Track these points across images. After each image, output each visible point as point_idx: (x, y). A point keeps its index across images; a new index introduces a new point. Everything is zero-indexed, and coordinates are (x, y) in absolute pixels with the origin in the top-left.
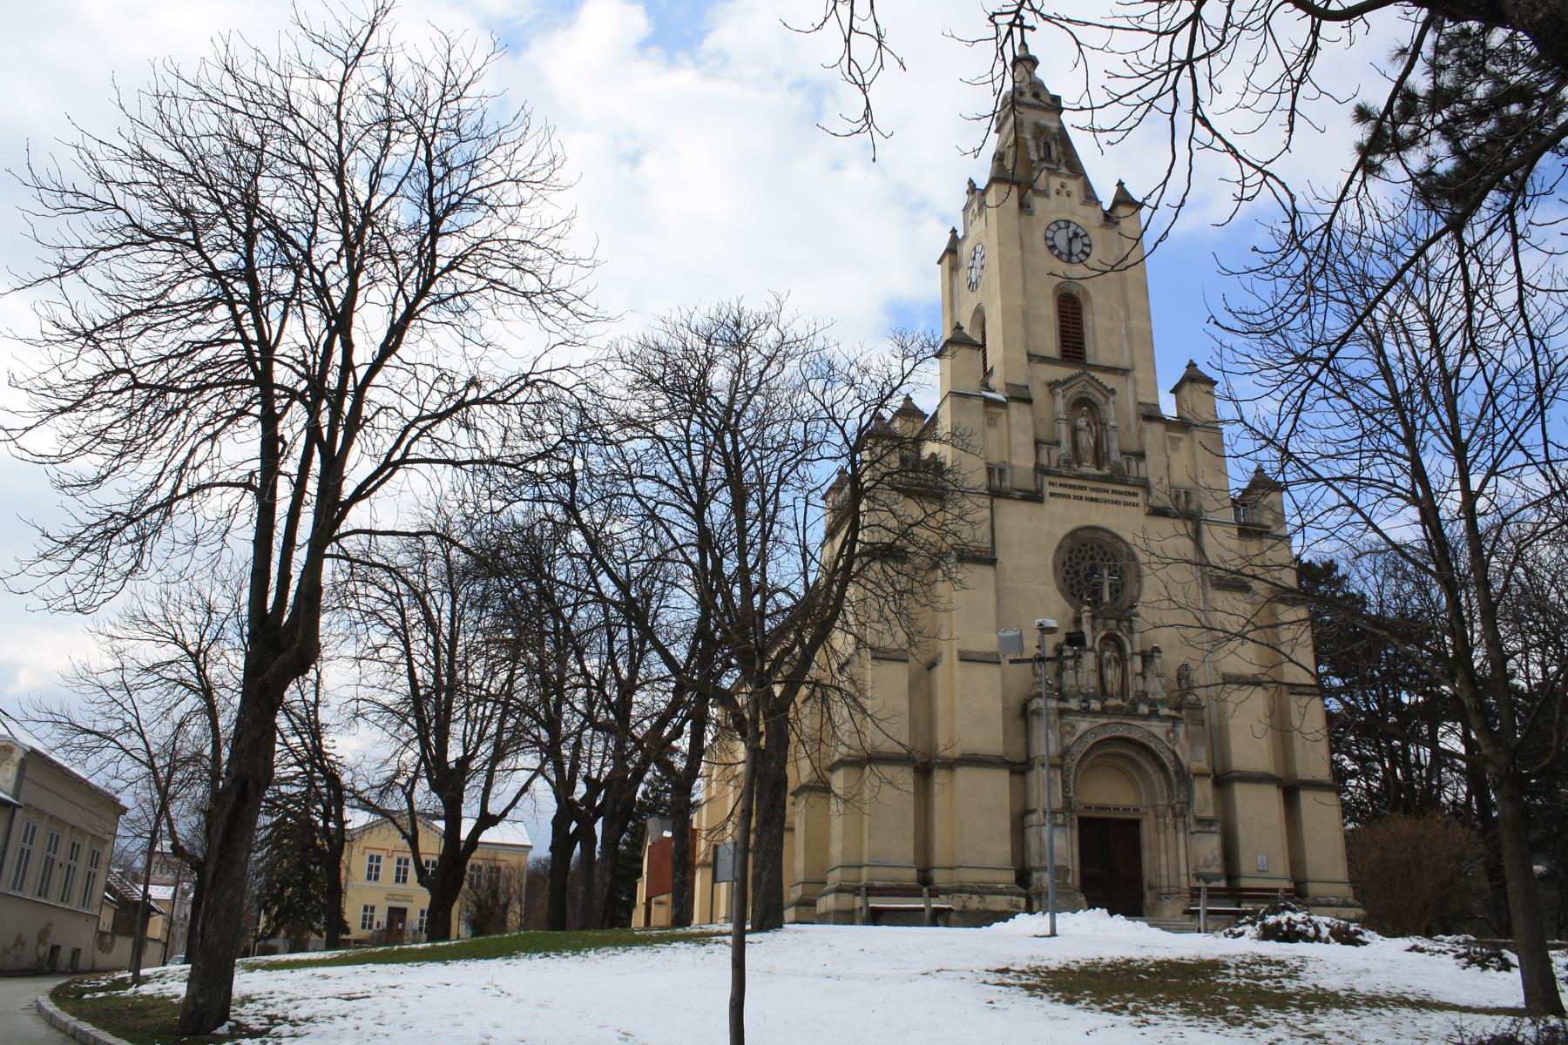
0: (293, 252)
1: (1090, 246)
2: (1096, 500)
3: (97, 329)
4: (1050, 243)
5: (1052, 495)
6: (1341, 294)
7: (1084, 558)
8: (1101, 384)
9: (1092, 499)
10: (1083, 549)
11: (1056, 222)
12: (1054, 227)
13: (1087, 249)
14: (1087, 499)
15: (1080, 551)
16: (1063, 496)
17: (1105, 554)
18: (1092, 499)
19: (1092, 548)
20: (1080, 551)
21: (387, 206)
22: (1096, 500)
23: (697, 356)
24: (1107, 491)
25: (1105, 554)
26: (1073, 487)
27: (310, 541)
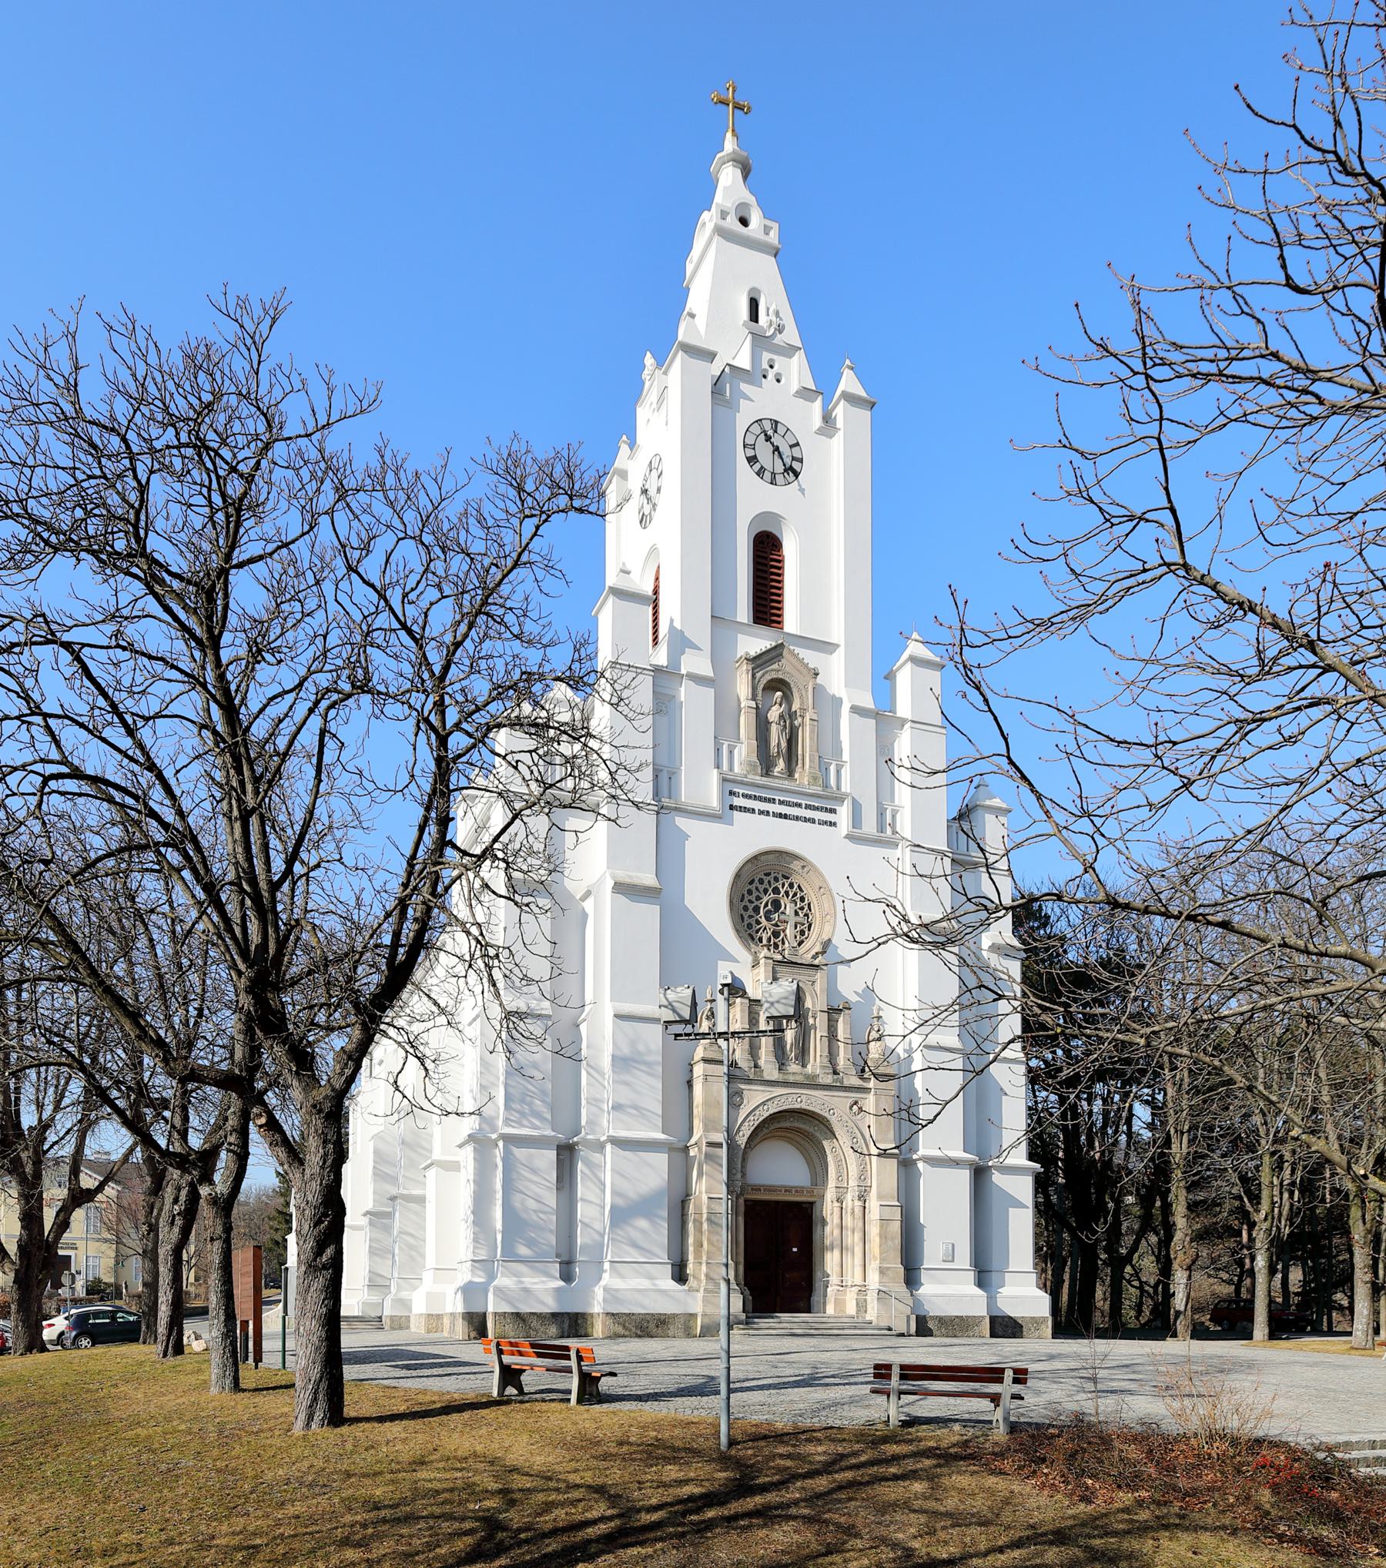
1: (801, 461)
2: (786, 817)
4: (750, 453)
6: (1281, 413)
8: (801, 661)
10: (766, 879)
14: (761, 812)
15: (750, 892)
16: (806, 820)
19: (761, 881)
20: (761, 881)
22: (786, 817)
23: (1264, 1008)
24: (800, 805)
25: (791, 885)
26: (760, 799)
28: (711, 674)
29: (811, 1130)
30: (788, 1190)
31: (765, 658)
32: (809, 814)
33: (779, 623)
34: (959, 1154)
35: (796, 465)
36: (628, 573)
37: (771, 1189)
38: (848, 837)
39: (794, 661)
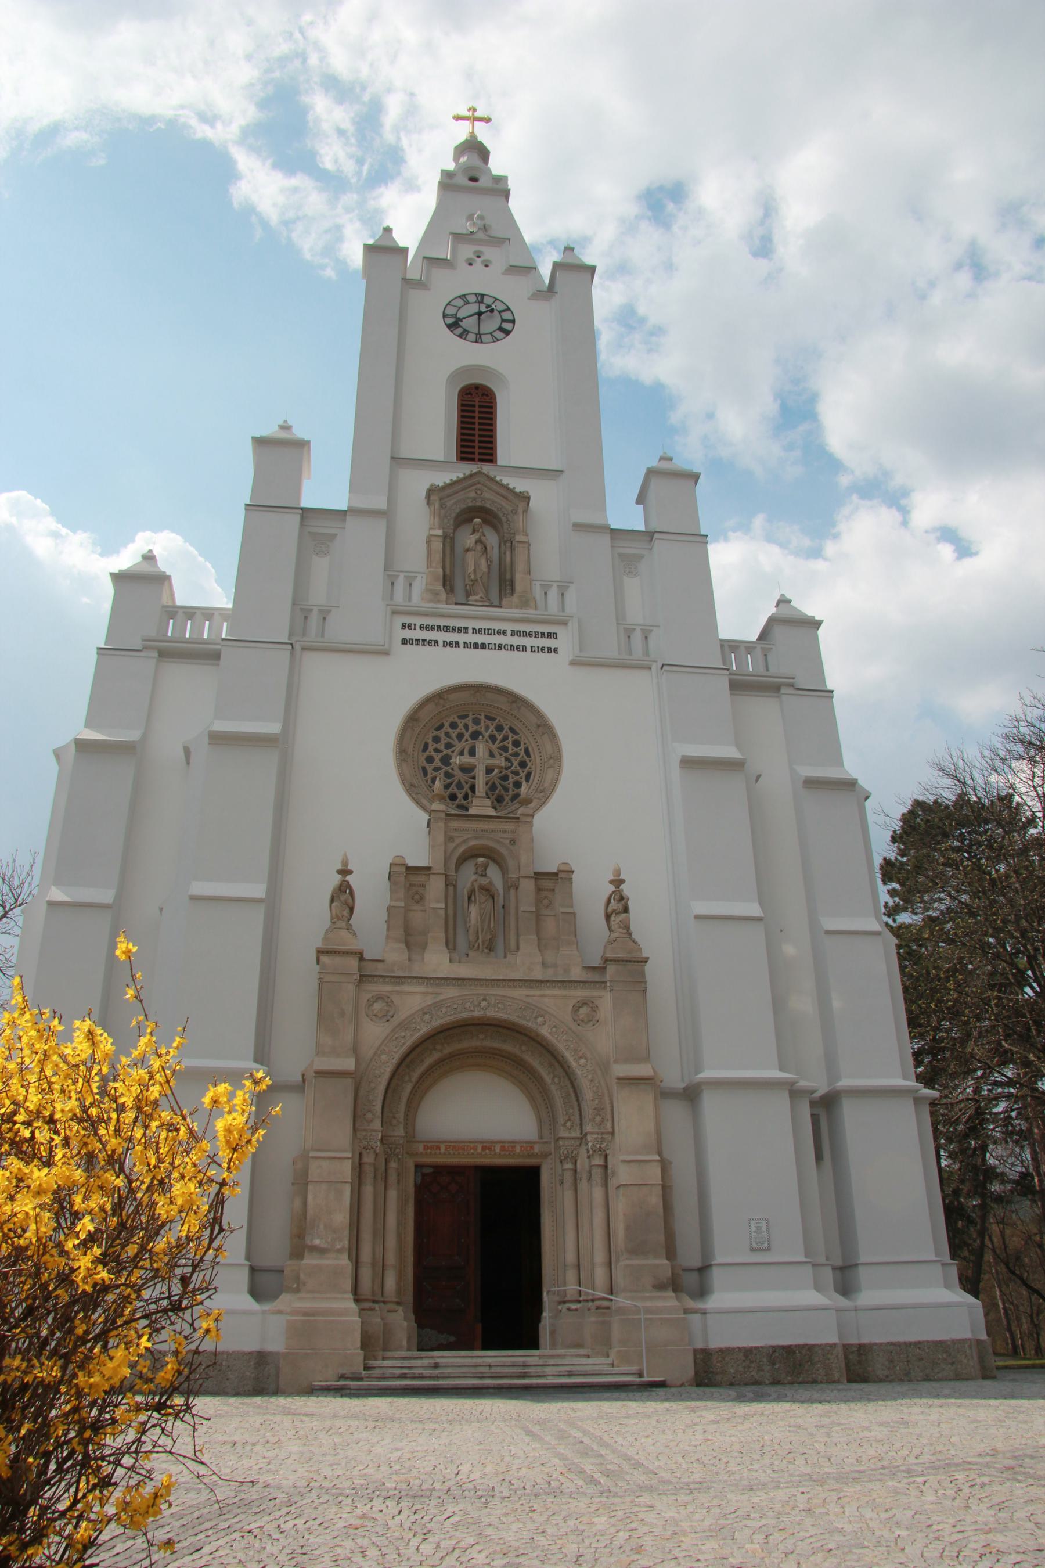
1: (513, 322)
2: (483, 646)
3: (143, 1480)
7: (460, 736)
9: (476, 646)
10: (441, 734)
12: (460, 302)
13: (507, 326)
17: (499, 728)
18: (476, 646)
22: (483, 646)
25: (499, 728)
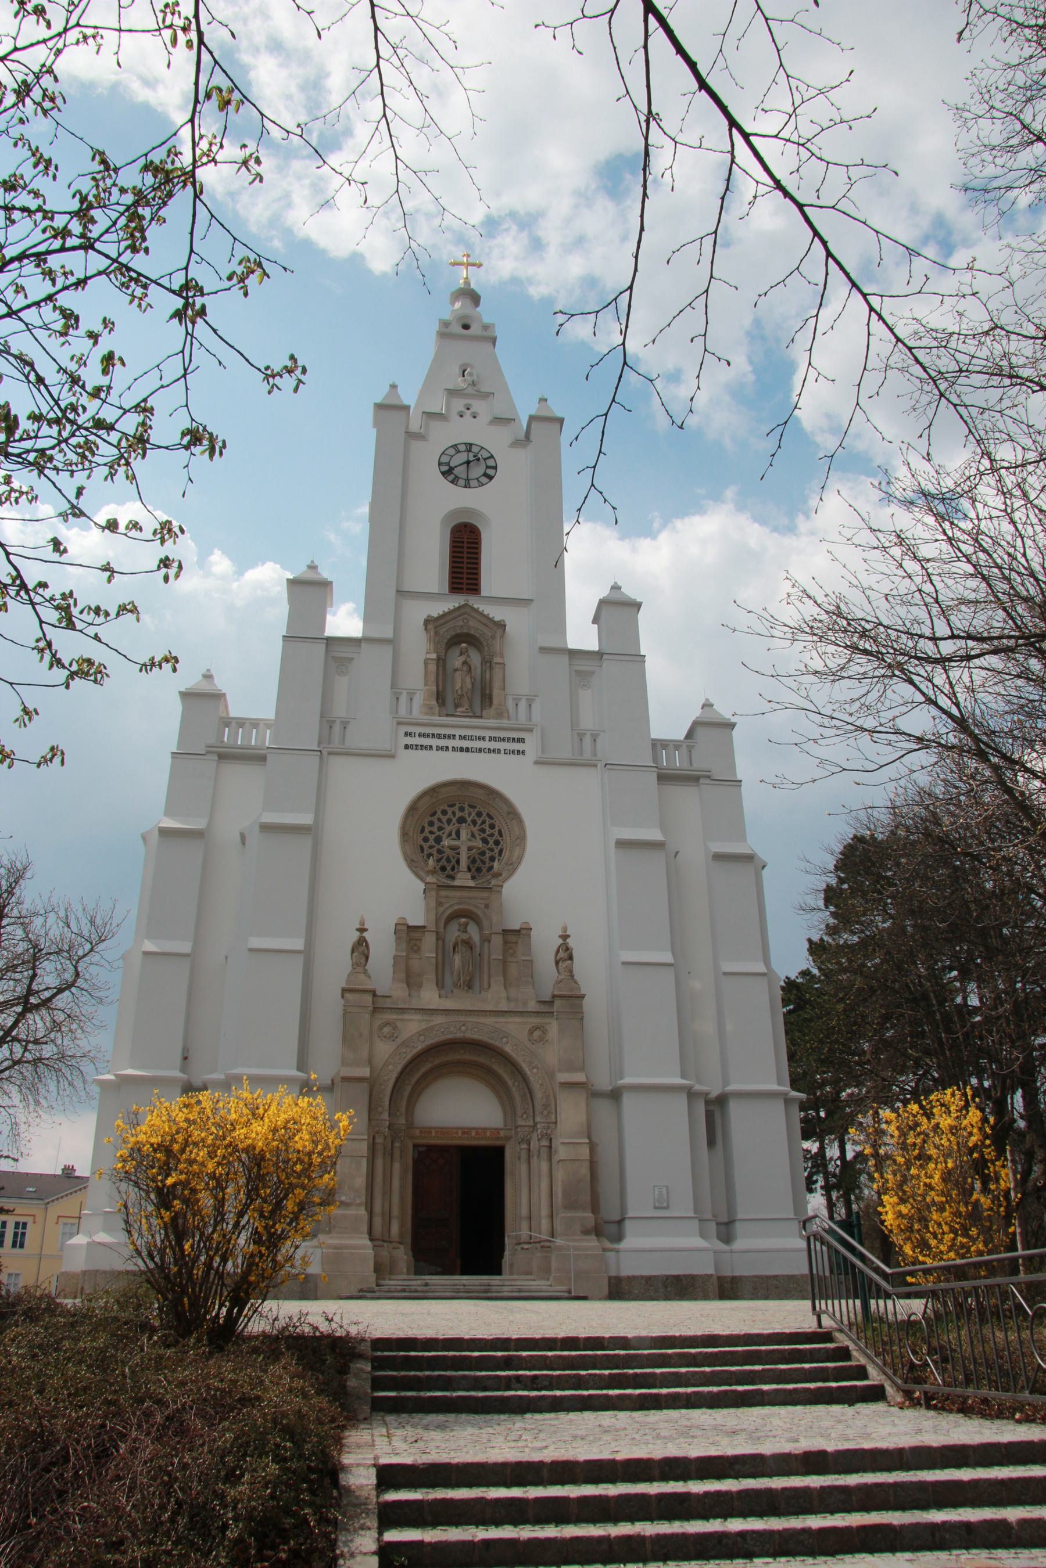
0: (112, 268)
1: (495, 468)
2: (467, 750)
5: (407, 747)
7: (449, 821)
9: (461, 749)
11: (455, 446)
13: (490, 472)
14: (439, 748)
17: (479, 814)
18: (461, 749)
21: (438, 64)
22: (467, 750)
24: (484, 739)
25: (479, 814)
26: (439, 736)
27: (282, 567)
28: (673, 961)
29: (510, 1083)
30: (466, 1131)
31: (448, 618)
32: (493, 745)
33: (476, 590)
34: (792, 1216)
35: (451, 477)
36: (546, 400)
37: (443, 1131)
38: (537, 763)
39: (476, 616)
